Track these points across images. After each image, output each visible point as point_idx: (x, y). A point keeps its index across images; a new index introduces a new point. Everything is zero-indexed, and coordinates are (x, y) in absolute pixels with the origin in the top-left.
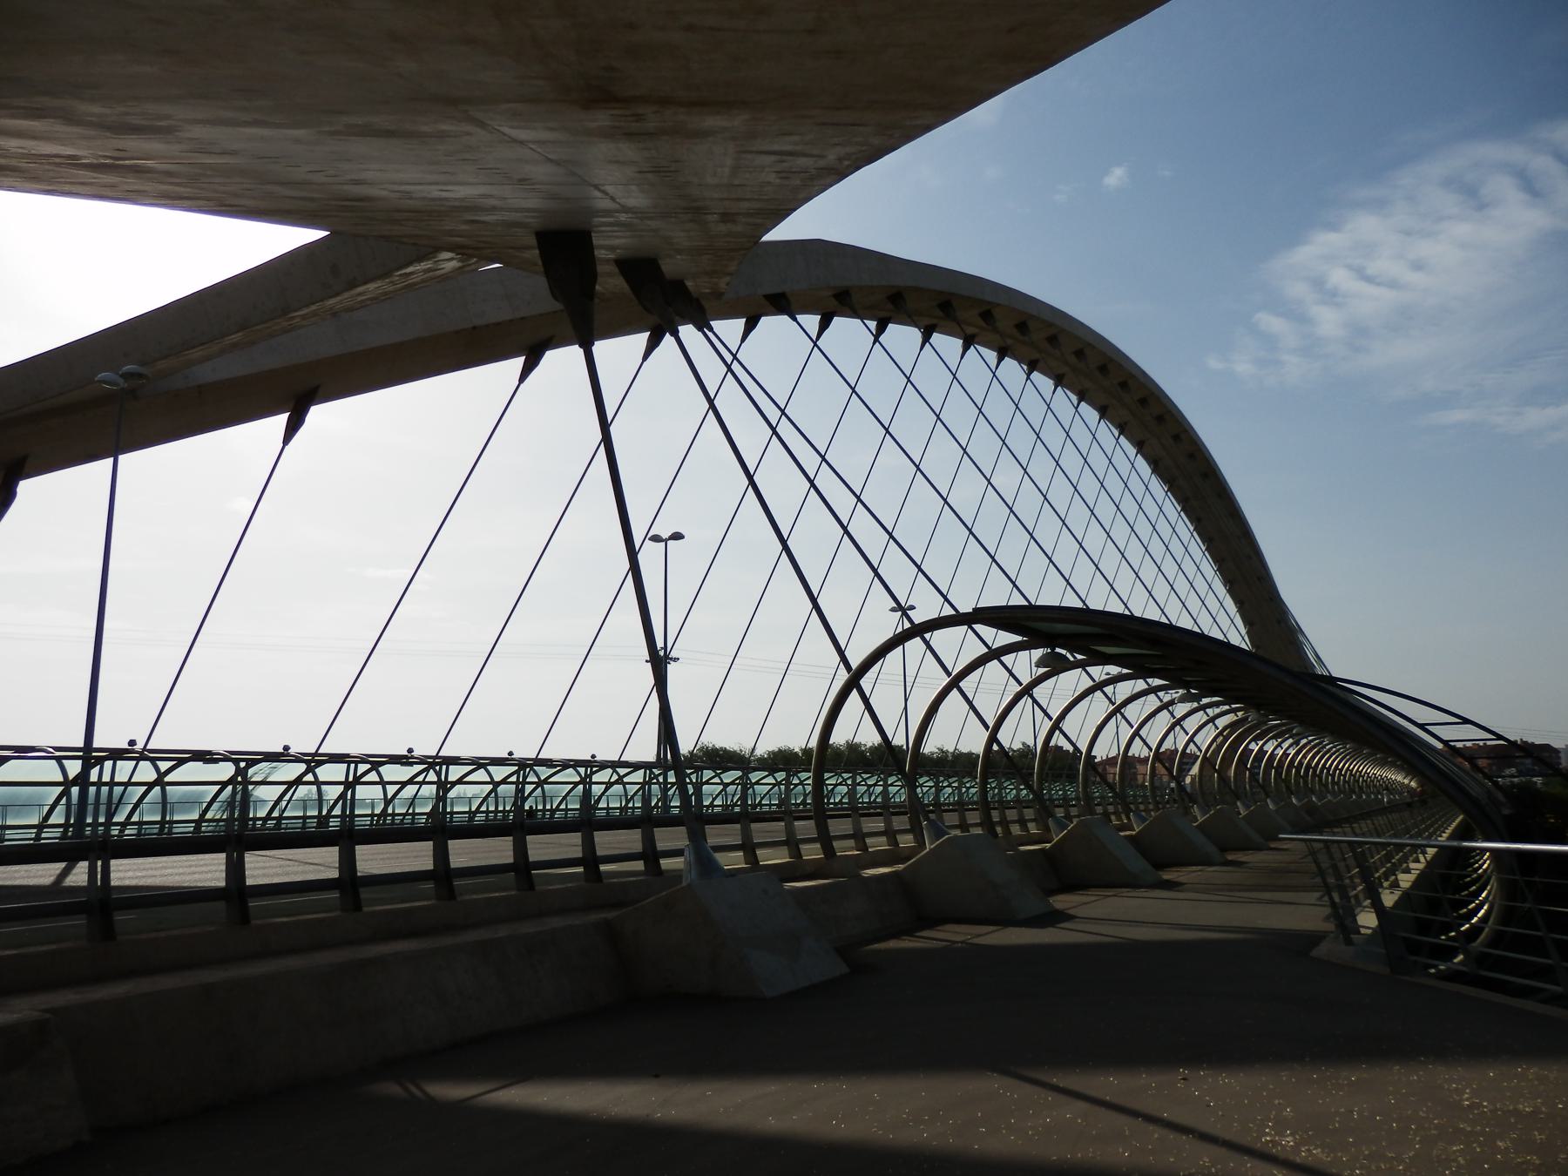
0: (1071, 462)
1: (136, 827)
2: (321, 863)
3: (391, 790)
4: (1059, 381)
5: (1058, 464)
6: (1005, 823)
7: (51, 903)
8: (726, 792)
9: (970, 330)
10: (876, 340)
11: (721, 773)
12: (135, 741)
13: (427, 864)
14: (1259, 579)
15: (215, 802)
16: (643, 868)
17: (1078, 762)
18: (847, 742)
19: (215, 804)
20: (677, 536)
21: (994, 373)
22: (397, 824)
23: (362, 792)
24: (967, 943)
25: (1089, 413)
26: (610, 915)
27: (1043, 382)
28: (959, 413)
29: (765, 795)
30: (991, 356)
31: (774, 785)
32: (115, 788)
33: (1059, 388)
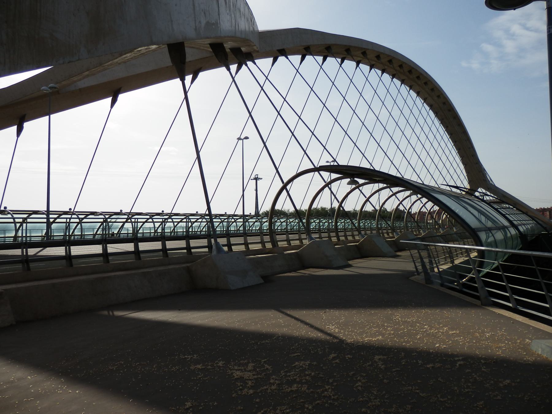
0: (406, 112)
1: (41, 238)
2: (157, 245)
3: (176, 224)
4: (403, 82)
5: (370, 107)
6: (383, 233)
7: (13, 260)
8: (282, 225)
9: (373, 63)
10: (341, 66)
11: (341, 220)
12: (6, 207)
13: (160, 247)
14: (473, 156)
15: (76, 229)
16: (208, 251)
17: (405, 214)
18: (321, 207)
19: (120, 227)
20: (247, 138)
21: (380, 79)
22: (159, 236)
23: (168, 225)
24: (310, 274)
25: (413, 94)
26: (188, 265)
27: (397, 82)
28: (368, 94)
29: (279, 226)
30: (380, 72)
31: (221, 222)
32: (70, 224)
33: (403, 85)
